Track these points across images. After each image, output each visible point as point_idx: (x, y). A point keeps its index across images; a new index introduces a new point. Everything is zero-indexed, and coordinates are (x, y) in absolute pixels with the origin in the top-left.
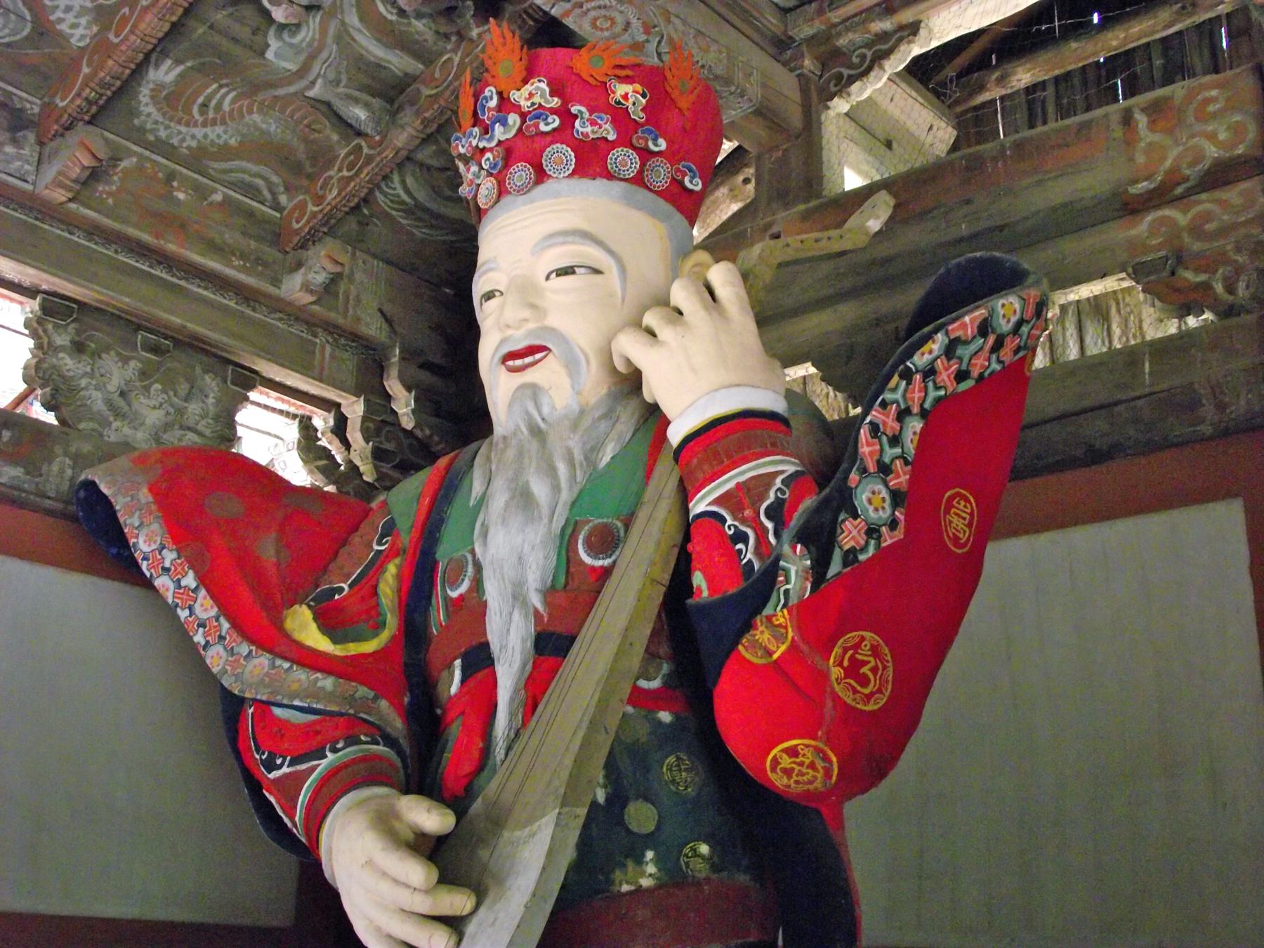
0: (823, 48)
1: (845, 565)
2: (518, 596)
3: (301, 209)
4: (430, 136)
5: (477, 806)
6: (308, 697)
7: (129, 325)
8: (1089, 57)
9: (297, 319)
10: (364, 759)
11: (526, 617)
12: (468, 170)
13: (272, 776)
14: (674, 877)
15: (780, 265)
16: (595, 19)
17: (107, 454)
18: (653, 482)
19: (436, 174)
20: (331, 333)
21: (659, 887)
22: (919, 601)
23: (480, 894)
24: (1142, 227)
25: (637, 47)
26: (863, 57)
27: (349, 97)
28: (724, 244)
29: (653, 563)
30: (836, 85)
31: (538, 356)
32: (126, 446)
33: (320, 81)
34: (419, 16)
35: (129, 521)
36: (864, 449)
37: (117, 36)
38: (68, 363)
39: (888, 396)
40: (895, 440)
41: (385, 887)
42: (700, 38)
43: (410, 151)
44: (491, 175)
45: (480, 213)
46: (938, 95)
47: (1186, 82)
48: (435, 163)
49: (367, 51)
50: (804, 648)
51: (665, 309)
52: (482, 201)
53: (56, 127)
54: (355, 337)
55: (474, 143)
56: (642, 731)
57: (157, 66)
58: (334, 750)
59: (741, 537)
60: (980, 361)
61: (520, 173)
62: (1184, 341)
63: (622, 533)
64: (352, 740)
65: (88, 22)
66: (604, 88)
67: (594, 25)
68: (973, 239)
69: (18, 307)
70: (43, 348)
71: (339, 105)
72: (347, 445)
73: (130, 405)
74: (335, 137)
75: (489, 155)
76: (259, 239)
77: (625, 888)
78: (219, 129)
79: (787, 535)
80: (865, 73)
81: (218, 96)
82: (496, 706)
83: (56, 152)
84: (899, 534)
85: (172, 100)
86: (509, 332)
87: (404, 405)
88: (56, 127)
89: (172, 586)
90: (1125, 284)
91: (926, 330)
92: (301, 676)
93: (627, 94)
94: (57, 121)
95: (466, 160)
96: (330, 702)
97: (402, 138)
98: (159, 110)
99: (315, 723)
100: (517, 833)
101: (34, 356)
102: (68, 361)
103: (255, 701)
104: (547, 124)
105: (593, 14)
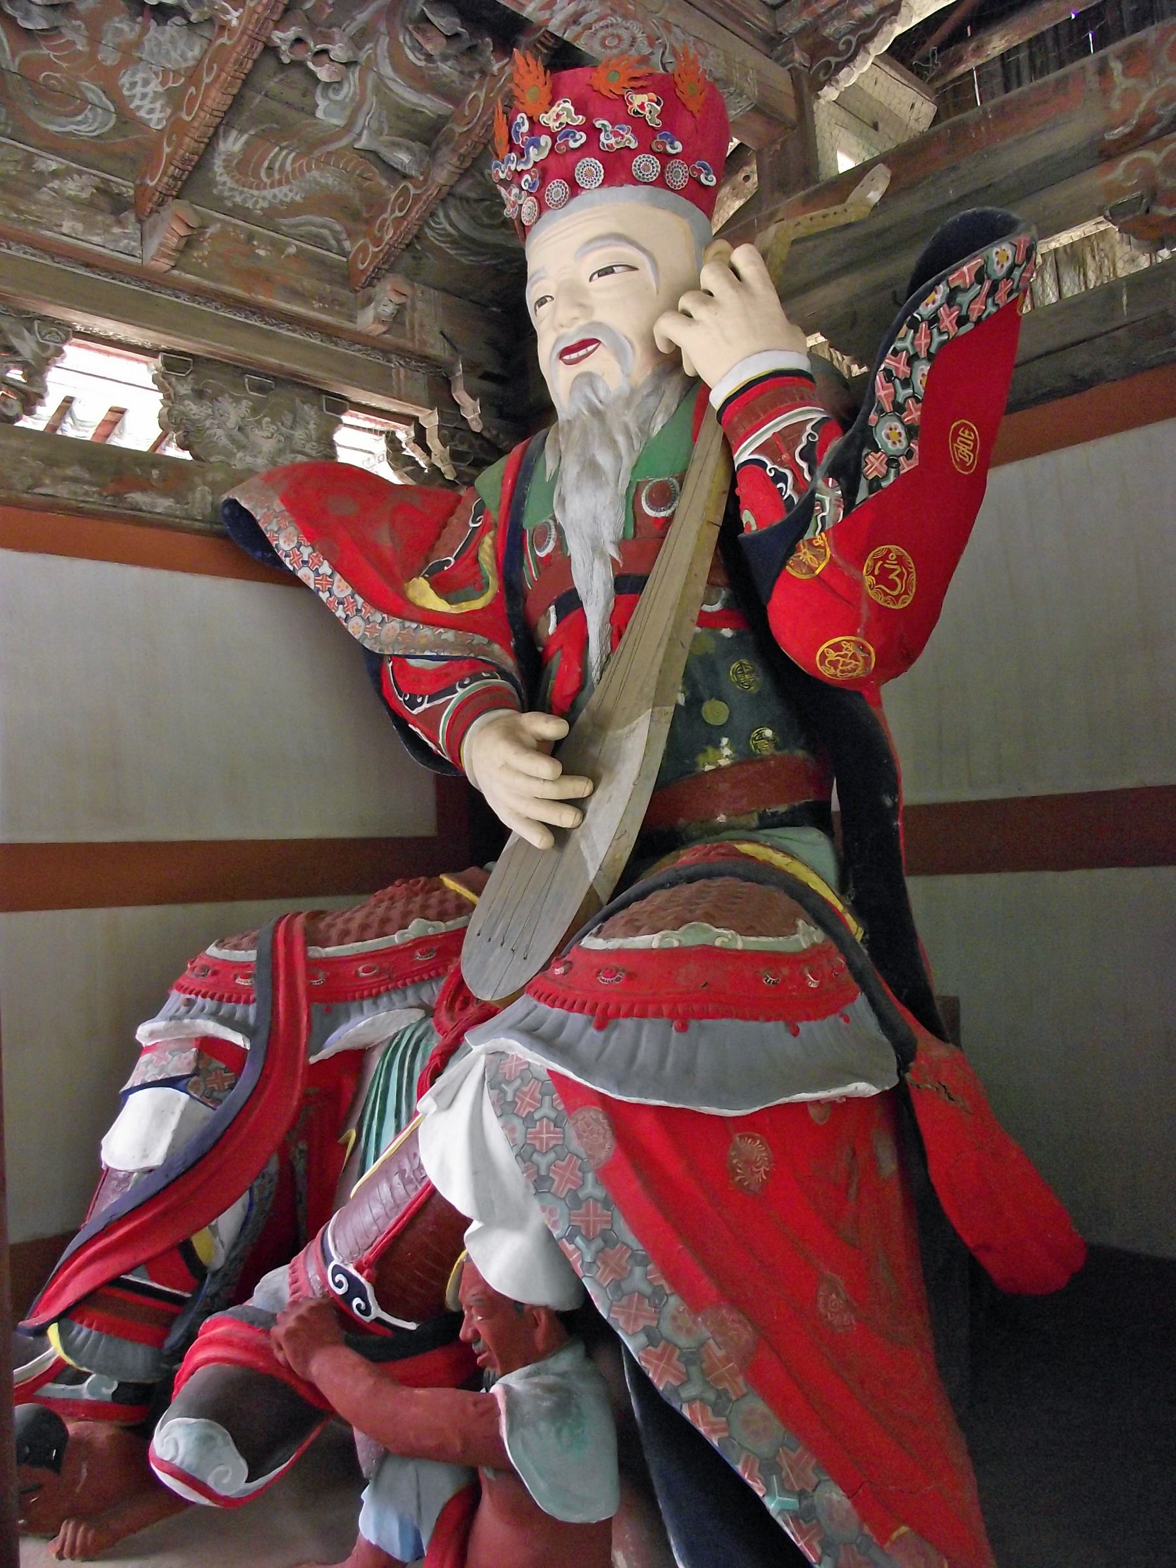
0: (811, 40)
1: (871, 491)
2: (596, 549)
3: (364, 252)
4: (467, 170)
5: (583, 716)
6: (436, 647)
7: (237, 371)
8: (1060, 16)
9: (373, 348)
10: (487, 690)
11: (605, 564)
12: (510, 193)
13: (415, 712)
14: (746, 758)
15: (794, 242)
16: (604, 38)
17: (238, 478)
18: (699, 443)
19: (475, 206)
20: (403, 357)
21: (732, 765)
22: (933, 517)
23: (596, 781)
24: (1118, 171)
25: (644, 60)
26: (849, 43)
27: (394, 144)
28: (738, 231)
29: (706, 508)
30: (825, 75)
31: (590, 348)
32: (251, 472)
33: (365, 132)
34: (445, 58)
35: (269, 527)
36: (880, 393)
37: (189, 114)
38: (193, 408)
39: (898, 345)
40: (907, 383)
41: (521, 782)
42: (699, 45)
43: (452, 187)
44: (530, 194)
45: (525, 230)
46: (919, 75)
47: (1157, 25)
48: (472, 195)
49: (403, 99)
50: (840, 562)
51: (696, 292)
52: (525, 220)
53: (150, 205)
54: (424, 358)
55: (513, 168)
56: (710, 645)
57: (225, 138)
58: (463, 686)
59: (781, 478)
60: (978, 306)
61: (556, 189)
62: (1157, 274)
63: (678, 489)
64: (476, 677)
65: (162, 106)
66: (623, 101)
67: (604, 46)
68: (960, 202)
69: (144, 366)
70: (171, 398)
71: (385, 152)
72: (427, 451)
73: (247, 437)
74: (384, 183)
75: (527, 177)
76: (331, 282)
77: (708, 768)
78: (285, 189)
79: (819, 472)
80: (851, 59)
81: (281, 158)
82: (588, 638)
83: (154, 227)
84: (915, 462)
85: (243, 167)
86: (563, 331)
87: (471, 411)
88: (150, 205)
89: (312, 575)
90: (1102, 228)
91: (929, 282)
92: (427, 632)
93: (643, 104)
94: (150, 200)
95: (506, 183)
96: (455, 649)
97: (442, 176)
98: (233, 177)
99: (440, 669)
100: (620, 732)
101: (165, 406)
102: (193, 406)
103: (393, 657)
104: (576, 141)
105: (602, 33)
